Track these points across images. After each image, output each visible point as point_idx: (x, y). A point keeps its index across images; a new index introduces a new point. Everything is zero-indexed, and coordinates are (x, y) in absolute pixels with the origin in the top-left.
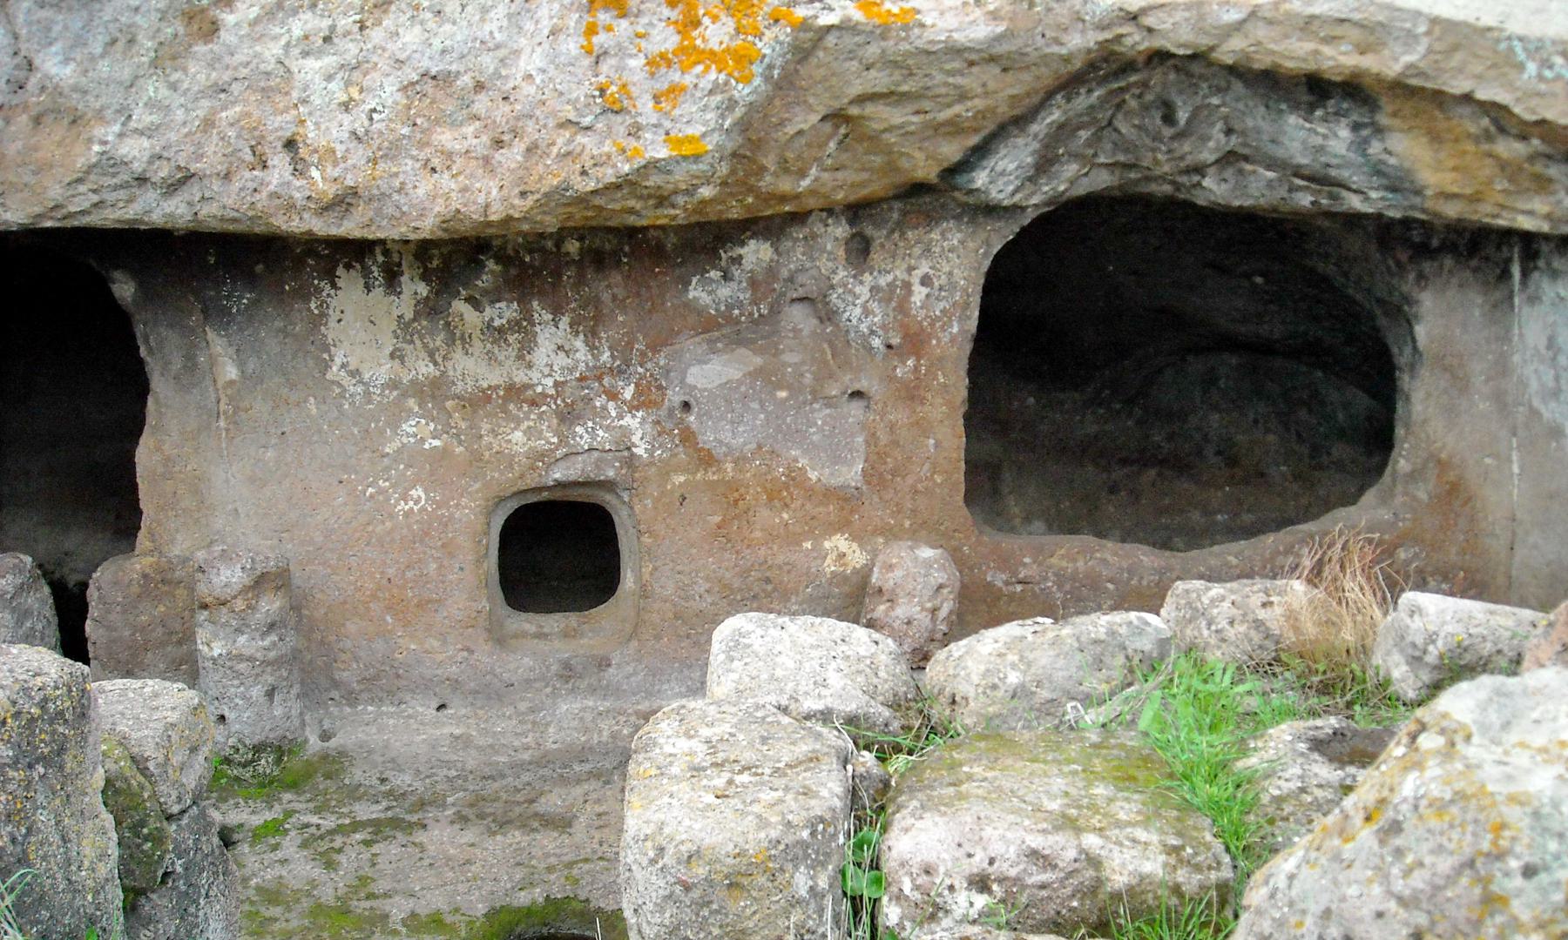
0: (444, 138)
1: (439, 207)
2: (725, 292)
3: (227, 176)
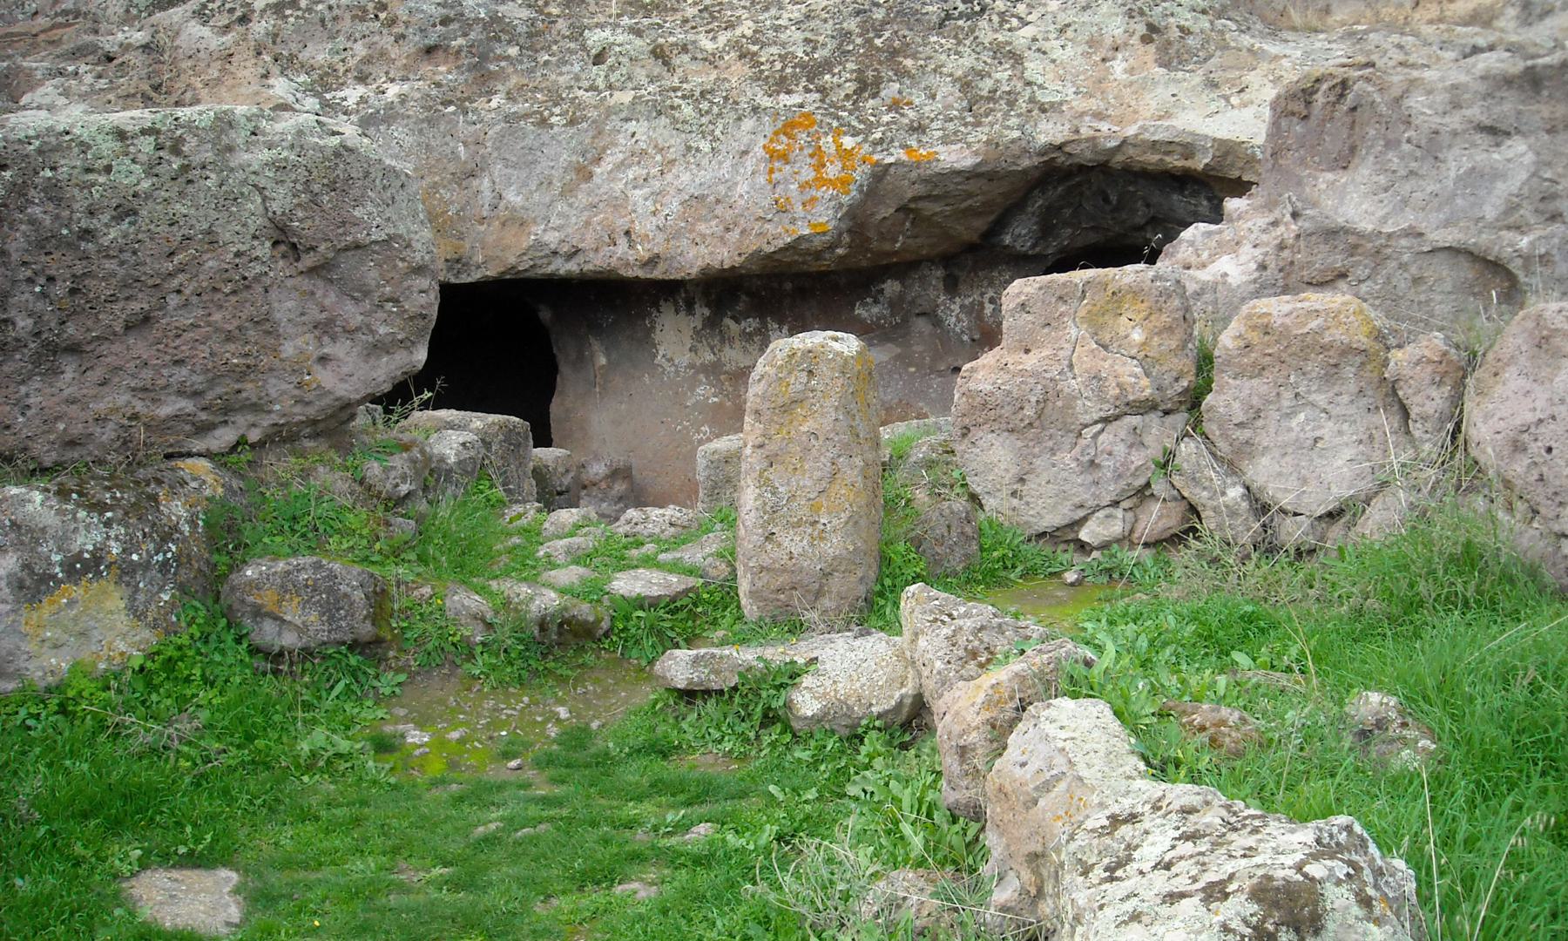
0: (702, 227)
2: (875, 310)
3: (597, 250)
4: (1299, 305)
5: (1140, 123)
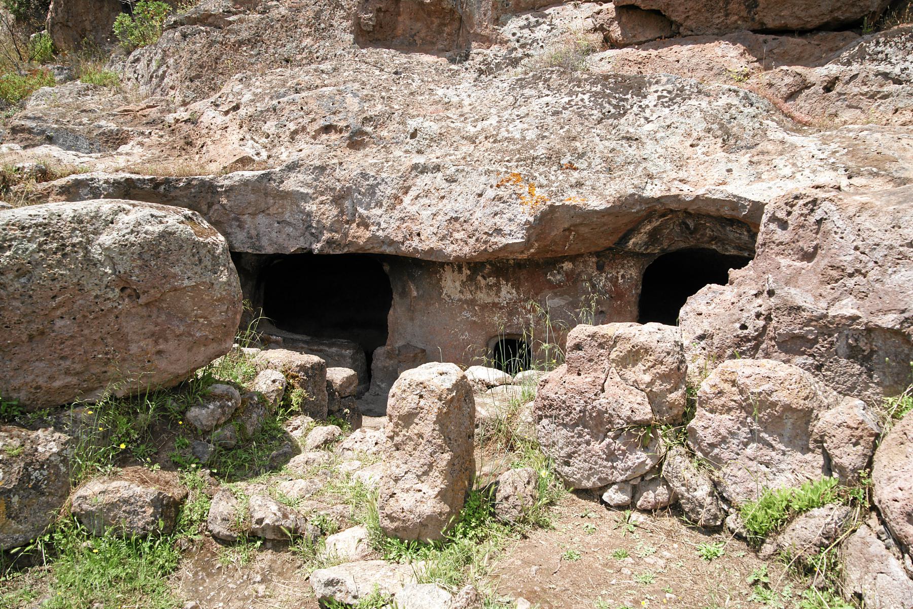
1: (454, 254)
2: (558, 277)
4: (757, 370)
5: (707, 187)
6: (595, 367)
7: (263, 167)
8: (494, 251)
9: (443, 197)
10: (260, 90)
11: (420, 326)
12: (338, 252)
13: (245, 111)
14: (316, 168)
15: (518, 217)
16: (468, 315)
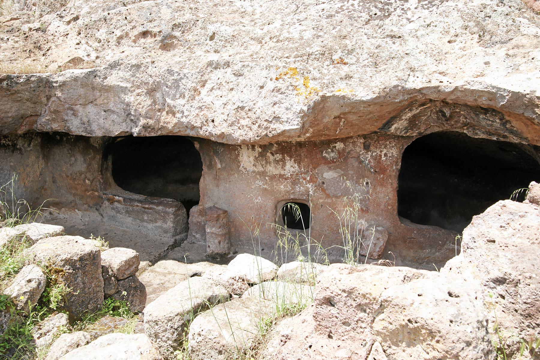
1: (241, 138)
2: (332, 155)
5: (465, 79)
6: (352, 334)
7: (91, 65)
8: (274, 136)
9: (232, 89)
10: (95, 4)
11: (223, 191)
12: (153, 135)
13: (83, 21)
14: (133, 66)
15: (294, 106)
16: (261, 183)
